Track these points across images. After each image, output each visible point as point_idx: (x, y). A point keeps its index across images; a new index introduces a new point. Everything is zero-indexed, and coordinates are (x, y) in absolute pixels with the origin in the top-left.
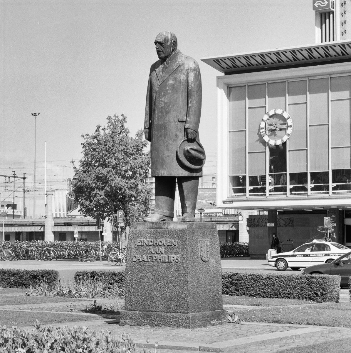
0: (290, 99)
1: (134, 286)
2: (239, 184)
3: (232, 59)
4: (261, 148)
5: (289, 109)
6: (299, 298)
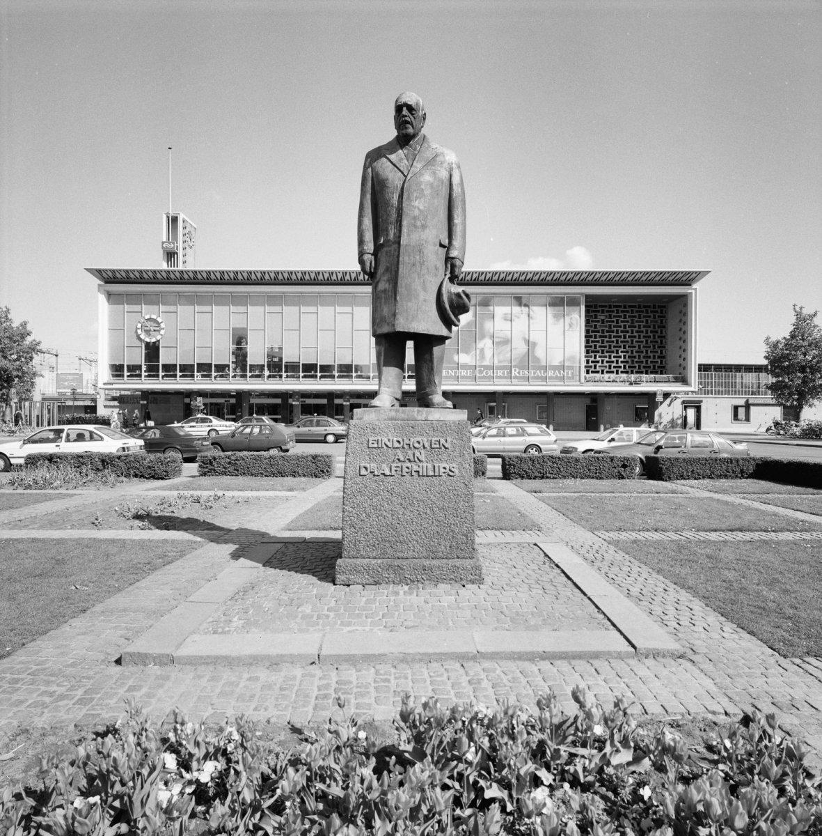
0: (163, 308)
2: (117, 371)
3: (113, 271)
4: (138, 343)
6: (304, 476)
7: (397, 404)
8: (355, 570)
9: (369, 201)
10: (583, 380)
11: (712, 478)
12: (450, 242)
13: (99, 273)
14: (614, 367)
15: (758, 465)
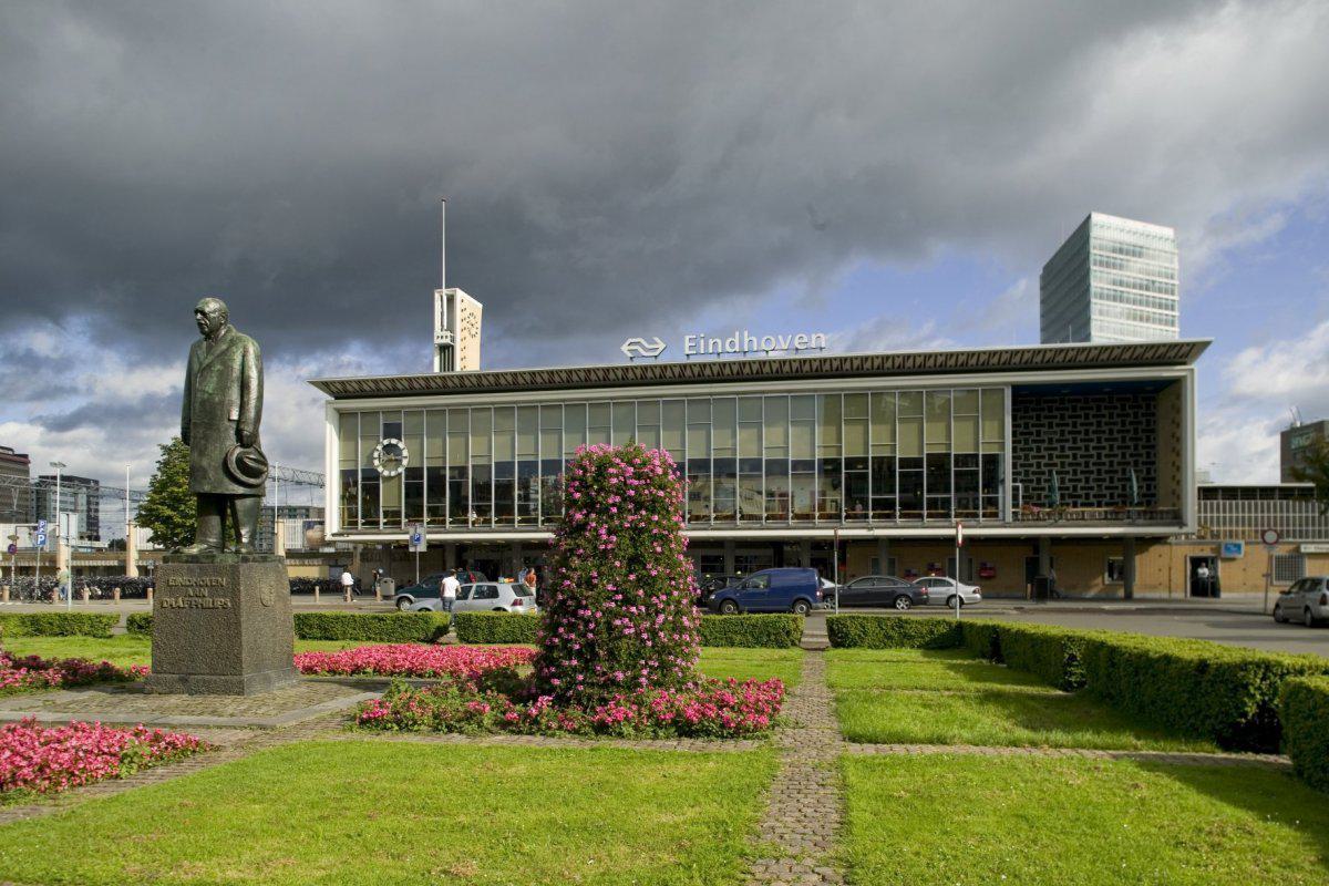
10: (1009, 518)
13: (326, 386)
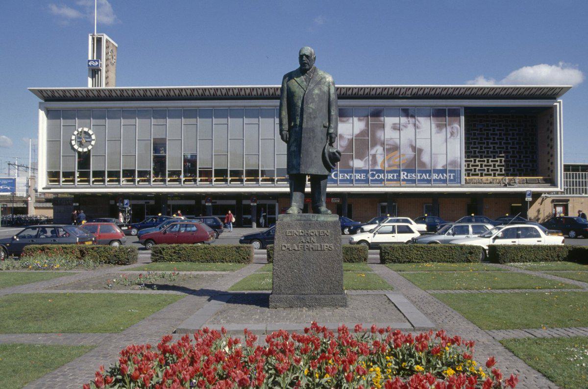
1: (284, 272)
4: (72, 153)
5: (93, 128)
6: (230, 262)
7: (301, 211)
8: (280, 301)
9: (286, 102)
10: (463, 182)
11: (536, 261)
12: (329, 125)
13: (40, 93)
14: (492, 170)
15: (570, 251)
